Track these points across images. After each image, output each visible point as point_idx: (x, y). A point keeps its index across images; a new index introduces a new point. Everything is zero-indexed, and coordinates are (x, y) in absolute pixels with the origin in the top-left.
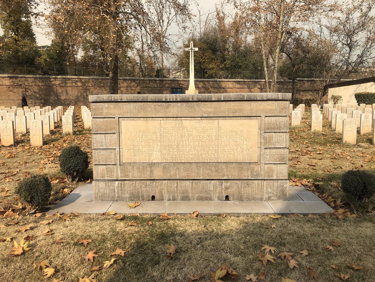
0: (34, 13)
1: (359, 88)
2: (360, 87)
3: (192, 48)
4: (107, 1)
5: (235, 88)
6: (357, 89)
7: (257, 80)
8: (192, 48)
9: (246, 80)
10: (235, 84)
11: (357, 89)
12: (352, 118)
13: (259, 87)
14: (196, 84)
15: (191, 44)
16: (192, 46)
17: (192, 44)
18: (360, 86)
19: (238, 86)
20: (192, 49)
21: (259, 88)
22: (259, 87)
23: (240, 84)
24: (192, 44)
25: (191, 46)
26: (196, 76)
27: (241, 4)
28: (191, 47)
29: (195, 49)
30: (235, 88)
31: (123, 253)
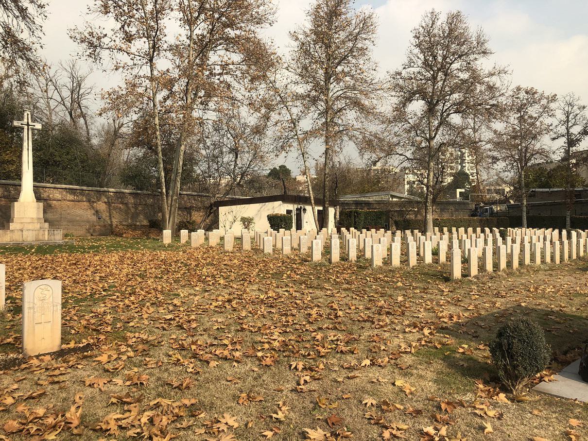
0: (548, 98)
1: (263, 208)
2: (265, 206)
3: (28, 123)
4: (143, 6)
5: (65, 200)
6: (261, 208)
7: (102, 189)
8: (28, 123)
9: (85, 188)
10: (64, 193)
11: (261, 208)
12: (380, 243)
13: (106, 200)
14: (36, 190)
15: (25, 114)
16: (28, 119)
17: (28, 115)
18: (265, 205)
19: (71, 197)
20: (28, 125)
21: (105, 203)
22: (106, 200)
23: (74, 194)
24: (28, 115)
25: (26, 117)
26: (37, 177)
27: (126, 65)
28: (26, 120)
29: (34, 126)
30: (65, 200)
31: (156, 438)
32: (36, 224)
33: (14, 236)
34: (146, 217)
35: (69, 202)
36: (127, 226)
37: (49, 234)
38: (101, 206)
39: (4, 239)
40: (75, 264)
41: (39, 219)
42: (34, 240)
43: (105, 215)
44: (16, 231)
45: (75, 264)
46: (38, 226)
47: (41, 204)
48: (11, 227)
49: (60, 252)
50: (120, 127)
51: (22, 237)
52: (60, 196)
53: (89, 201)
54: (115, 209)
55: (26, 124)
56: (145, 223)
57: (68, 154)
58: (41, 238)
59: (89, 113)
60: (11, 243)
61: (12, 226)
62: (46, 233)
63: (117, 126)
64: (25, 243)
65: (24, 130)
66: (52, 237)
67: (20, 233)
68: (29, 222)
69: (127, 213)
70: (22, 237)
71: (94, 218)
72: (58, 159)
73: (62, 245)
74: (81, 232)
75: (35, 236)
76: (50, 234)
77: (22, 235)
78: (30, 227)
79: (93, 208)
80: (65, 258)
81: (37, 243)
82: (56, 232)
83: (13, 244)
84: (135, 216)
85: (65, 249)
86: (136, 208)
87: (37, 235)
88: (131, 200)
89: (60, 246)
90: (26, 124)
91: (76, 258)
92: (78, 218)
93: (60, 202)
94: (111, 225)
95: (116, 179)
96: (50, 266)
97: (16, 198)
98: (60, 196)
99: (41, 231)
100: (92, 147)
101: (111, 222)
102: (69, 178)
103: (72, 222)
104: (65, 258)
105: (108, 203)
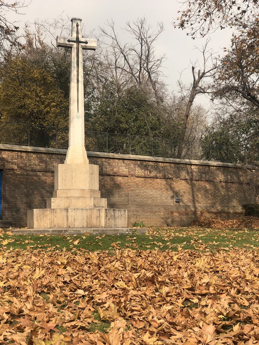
3: (77, 38)
5: (132, 175)
9: (160, 159)
10: (132, 166)
19: (139, 171)
23: (146, 168)
30: (132, 175)
32: (88, 200)
33: (55, 219)
34: (240, 201)
35: (137, 179)
36: (215, 213)
37: (106, 216)
38: (181, 186)
39: (42, 224)
40: (152, 281)
41: (92, 191)
42: (85, 225)
43: (186, 199)
44: (58, 211)
45: (152, 281)
46: (90, 203)
47: (96, 168)
48: (52, 204)
49: (123, 246)
50: (200, 78)
51: (67, 220)
52: (127, 170)
53: (165, 178)
54: (199, 190)
55: (75, 40)
56: (240, 209)
57: (136, 120)
58: (95, 222)
59: (159, 80)
60: (51, 230)
61: (55, 202)
62: (103, 214)
63: (197, 78)
64: (71, 231)
65: (73, 49)
66: (112, 221)
67: (64, 213)
68: (78, 196)
69: (214, 196)
70: (67, 220)
71: (171, 202)
72: (124, 126)
73: (127, 235)
74: (155, 220)
75: (85, 218)
76: (109, 215)
77: (67, 217)
78: (80, 204)
79: (172, 188)
80: (128, 261)
81: (89, 230)
82: (117, 213)
83: (53, 231)
84: (226, 200)
85: (130, 241)
86: (228, 189)
87: (90, 218)
88: (221, 177)
89: (123, 237)
90: (75, 40)
91: (152, 263)
92: (150, 202)
93: (126, 178)
94: (195, 213)
95: (199, 151)
96: (86, 284)
97: (62, 158)
98: (127, 170)
99: (95, 211)
100: (165, 110)
101: (195, 207)
102: (137, 148)
103: (142, 206)
104: (128, 261)
105: (191, 181)
